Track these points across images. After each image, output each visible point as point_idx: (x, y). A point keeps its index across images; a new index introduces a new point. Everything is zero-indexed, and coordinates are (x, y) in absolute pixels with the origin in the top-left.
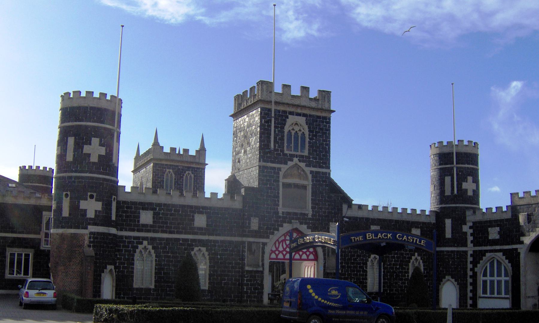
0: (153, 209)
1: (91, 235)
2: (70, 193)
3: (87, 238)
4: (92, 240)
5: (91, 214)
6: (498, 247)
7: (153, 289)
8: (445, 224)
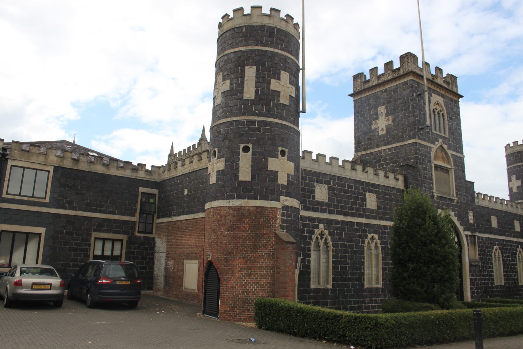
0: (328, 183)
1: (284, 211)
2: (253, 146)
3: (279, 214)
4: (285, 218)
5: (282, 180)
7: (331, 289)
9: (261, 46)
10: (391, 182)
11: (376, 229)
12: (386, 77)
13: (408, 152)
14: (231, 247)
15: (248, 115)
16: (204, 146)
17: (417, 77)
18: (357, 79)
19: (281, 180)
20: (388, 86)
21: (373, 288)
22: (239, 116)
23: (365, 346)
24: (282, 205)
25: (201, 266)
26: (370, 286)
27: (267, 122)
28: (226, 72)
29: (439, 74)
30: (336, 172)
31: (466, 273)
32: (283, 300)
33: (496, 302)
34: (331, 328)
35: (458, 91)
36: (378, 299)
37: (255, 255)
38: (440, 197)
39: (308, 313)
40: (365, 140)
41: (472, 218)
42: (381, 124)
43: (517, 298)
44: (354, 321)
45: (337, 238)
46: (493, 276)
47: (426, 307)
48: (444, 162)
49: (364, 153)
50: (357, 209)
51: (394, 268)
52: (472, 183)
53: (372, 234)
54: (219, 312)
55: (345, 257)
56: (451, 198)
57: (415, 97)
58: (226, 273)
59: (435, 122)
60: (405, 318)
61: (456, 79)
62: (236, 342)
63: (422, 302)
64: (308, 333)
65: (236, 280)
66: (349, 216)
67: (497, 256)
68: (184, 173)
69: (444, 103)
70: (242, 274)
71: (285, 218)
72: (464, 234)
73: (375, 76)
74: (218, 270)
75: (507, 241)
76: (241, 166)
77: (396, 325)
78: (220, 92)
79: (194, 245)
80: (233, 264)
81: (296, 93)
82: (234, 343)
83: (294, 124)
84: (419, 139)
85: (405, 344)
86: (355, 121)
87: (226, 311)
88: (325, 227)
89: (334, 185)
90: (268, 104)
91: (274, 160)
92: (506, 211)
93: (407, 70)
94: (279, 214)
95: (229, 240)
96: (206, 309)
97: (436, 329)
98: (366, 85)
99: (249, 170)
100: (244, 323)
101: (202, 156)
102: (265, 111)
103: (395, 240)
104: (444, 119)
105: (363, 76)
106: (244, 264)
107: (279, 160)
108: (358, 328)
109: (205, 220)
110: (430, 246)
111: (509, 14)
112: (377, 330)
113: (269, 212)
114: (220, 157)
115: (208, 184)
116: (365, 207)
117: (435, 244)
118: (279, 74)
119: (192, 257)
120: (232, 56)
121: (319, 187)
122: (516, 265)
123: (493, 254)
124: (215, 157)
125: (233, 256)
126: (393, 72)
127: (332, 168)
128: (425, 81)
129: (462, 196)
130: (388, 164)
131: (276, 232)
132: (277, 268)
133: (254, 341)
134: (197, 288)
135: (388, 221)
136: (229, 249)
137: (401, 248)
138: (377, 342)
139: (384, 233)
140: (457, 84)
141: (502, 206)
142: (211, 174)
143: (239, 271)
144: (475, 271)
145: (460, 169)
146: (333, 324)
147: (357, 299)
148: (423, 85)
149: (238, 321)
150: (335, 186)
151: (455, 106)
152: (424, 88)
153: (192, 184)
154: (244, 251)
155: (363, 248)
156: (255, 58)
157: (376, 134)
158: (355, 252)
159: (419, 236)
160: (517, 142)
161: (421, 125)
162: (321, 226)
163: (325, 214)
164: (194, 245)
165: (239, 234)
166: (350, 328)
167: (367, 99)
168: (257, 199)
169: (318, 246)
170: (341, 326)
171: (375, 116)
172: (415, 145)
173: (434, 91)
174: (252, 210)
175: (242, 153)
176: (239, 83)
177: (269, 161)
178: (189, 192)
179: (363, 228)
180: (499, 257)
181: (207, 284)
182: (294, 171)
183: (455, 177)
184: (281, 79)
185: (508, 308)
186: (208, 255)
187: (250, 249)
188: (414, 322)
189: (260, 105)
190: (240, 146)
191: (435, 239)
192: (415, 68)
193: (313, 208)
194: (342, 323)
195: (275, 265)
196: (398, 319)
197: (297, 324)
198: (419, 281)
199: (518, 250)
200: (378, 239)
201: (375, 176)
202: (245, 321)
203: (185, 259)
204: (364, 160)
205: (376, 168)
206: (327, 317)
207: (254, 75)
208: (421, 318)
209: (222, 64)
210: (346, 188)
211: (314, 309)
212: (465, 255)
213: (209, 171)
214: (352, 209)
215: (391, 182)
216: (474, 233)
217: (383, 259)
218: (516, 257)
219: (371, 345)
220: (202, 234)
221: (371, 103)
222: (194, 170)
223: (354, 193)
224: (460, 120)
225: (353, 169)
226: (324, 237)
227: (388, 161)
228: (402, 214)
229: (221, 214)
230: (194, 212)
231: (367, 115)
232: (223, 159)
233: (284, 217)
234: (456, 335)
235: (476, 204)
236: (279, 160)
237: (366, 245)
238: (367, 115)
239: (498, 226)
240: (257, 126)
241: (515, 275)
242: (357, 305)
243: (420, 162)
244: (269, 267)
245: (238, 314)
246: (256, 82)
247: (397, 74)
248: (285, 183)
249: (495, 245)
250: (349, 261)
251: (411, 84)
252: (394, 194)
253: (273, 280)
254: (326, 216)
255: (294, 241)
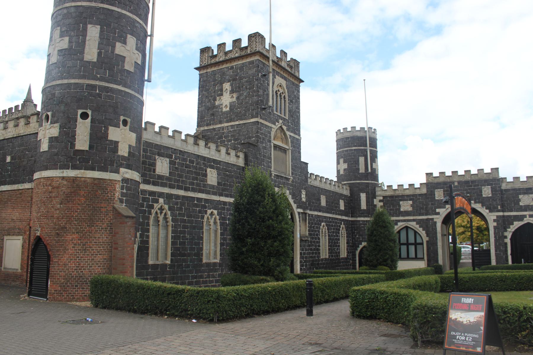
0: (170, 157)
1: (124, 183)
3: (118, 187)
4: (125, 191)
5: (123, 151)
6: (411, 218)
7: (169, 265)
8: (360, 197)
9: (107, 4)
10: (232, 159)
11: (216, 205)
12: (233, 54)
13: (249, 130)
14: (64, 221)
15: (89, 79)
16: (29, 108)
17: (263, 58)
18: (204, 52)
19: (122, 151)
20: (234, 64)
21: (211, 263)
22: (79, 79)
23: (207, 319)
24: (122, 178)
25: (26, 242)
26: (208, 261)
27: (110, 88)
28: (65, 27)
29: (284, 58)
30: (178, 145)
31: (297, 248)
32: (122, 277)
33: (321, 273)
34: (173, 303)
35: (299, 76)
36: (215, 273)
37: (91, 230)
38: (277, 175)
39: (149, 289)
40: (208, 116)
41: (304, 196)
42: (226, 101)
43: (338, 269)
44: (197, 295)
45: (177, 213)
46: (320, 250)
47: (262, 279)
48: (283, 143)
49: (206, 128)
50: (198, 185)
51: (233, 243)
52: (306, 164)
53: (212, 210)
54: (49, 292)
55: (184, 232)
56: (287, 177)
57: (260, 77)
58: (58, 249)
59: (277, 103)
60: (245, 290)
61: (299, 64)
62: (71, 324)
63: (258, 275)
64: (149, 309)
65: (70, 257)
66: (189, 191)
67: (324, 232)
68: (6, 138)
69: (287, 86)
70: (76, 250)
71: (125, 191)
72: (297, 211)
73: (222, 51)
74: (48, 246)
75: (333, 218)
76: (78, 133)
77: (237, 297)
78: (57, 49)
79: (17, 220)
80: (66, 240)
81: (142, 60)
82: (69, 325)
83: (138, 93)
84: (261, 118)
85: (245, 314)
86: (199, 95)
87: (56, 291)
88: (165, 202)
89: (176, 159)
90: (111, 69)
91: (115, 130)
92: (334, 191)
93: (254, 50)
94: (118, 186)
95: (62, 214)
96: (33, 290)
97: (273, 299)
98: (213, 60)
99: (87, 138)
100: (78, 303)
101: (31, 120)
102: (107, 76)
103: (235, 216)
104: (285, 101)
105: (211, 50)
106: (79, 240)
107: (121, 130)
108: (200, 302)
109: (32, 192)
110: (267, 222)
111: (346, 11)
112: (219, 303)
113: (107, 185)
114: (53, 122)
115: (38, 151)
116: (205, 183)
117: (273, 220)
118: (126, 38)
119: (15, 232)
120: (73, 10)
121: (160, 160)
122: (339, 240)
123: (321, 230)
124: (48, 122)
125: (66, 230)
126: (241, 50)
127: (175, 141)
128: (271, 62)
129: (297, 176)
130: (230, 141)
131: (115, 205)
132: (115, 244)
133: (91, 321)
134: (20, 266)
135: (228, 197)
136: (62, 223)
137: (240, 223)
138: (219, 314)
139: (223, 209)
140: (299, 69)
141: (331, 186)
142: (42, 140)
143: (73, 247)
144: (304, 246)
145: (297, 150)
146: (174, 299)
147: (196, 274)
148: (268, 66)
149: (71, 301)
150: (177, 160)
151: (296, 89)
152: (269, 69)
153: (16, 151)
154: (79, 226)
155: (203, 223)
156: (100, 16)
157: (220, 110)
158: (194, 228)
159: (258, 213)
160: (347, 128)
161: (264, 105)
162: (161, 200)
163: (166, 188)
164: (17, 220)
165: (73, 207)
166: (192, 302)
167: (213, 74)
168: (95, 170)
169: (157, 220)
170: (183, 300)
171: (219, 92)
172: (256, 124)
173: (278, 74)
174: (89, 181)
175: (79, 120)
176: (80, 42)
177: (109, 130)
178: (12, 159)
179: (203, 203)
180: (325, 233)
181: (34, 262)
182: (136, 143)
183: (291, 157)
184: (128, 43)
185: (332, 278)
186: (36, 230)
187: (86, 223)
188: (253, 293)
189: (102, 69)
190: (78, 111)
191: (272, 215)
192: (262, 49)
193: (153, 181)
194: (184, 298)
195: (112, 241)
196: (239, 291)
197: (137, 301)
198: (257, 255)
199: (341, 226)
200: (217, 215)
201: (217, 152)
202: (78, 300)
203: (6, 235)
204: (205, 136)
205: (218, 144)
206: (168, 292)
207: (98, 35)
208: (259, 290)
209: (60, 18)
210: (188, 163)
211: (155, 285)
212: (296, 231)
213: (40, 136)
214: (193, 184)
215: (232, 159)
216: (306, 210)
217: (222, 234)
218: (339, 233)
219: (213, 318)
220: (28, 206)
221: (217, 78)
222: (20, 135)
223: (195, 168)
224: (299, 104)
225: (196, 144)
226: (164, 212)
227: (230, 138)
228: (242, 191)
229: (53, 186)
230: (19, 183)
231: (212, 90)
232: (57, 125)
233: (124, 190)
234: (289, 304)
235: (309, 184)
236: (121, 130)
237: (206, 220)
238: (212, 90)
239: (326, 205)
240: (97, 91)
241: (337, 249)
242: (195, 280)
243: (260, 141)
244: (107, 242)
245: (71, 293)
246: (99, 44)
247: (244, 53)
248: (126, 155)
249: (323, 222)
250: (188, 237)
251: (257, 64)
252: (234, 171)
253: (111, 257)
254: (166, 190)
255: (134, 215)
